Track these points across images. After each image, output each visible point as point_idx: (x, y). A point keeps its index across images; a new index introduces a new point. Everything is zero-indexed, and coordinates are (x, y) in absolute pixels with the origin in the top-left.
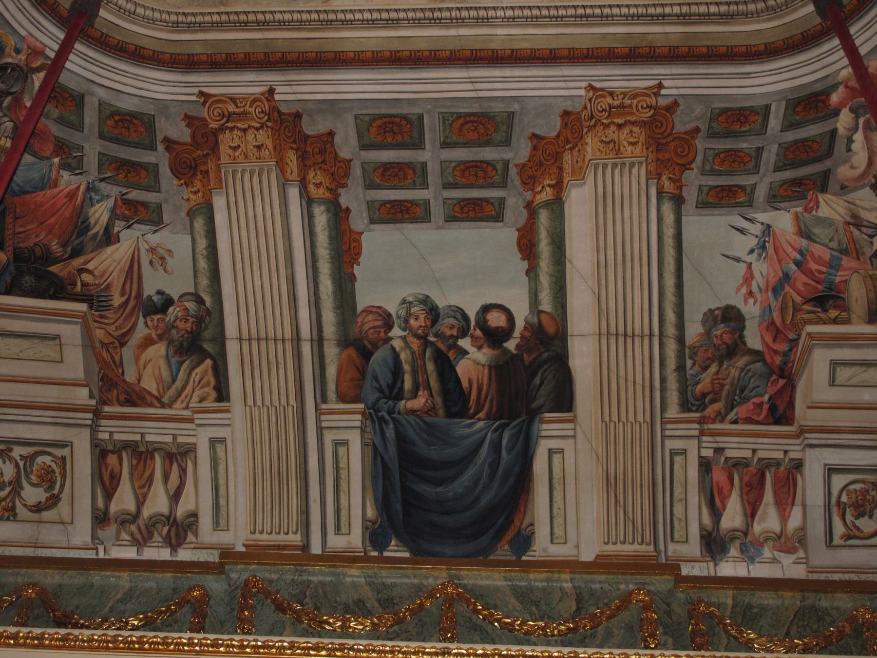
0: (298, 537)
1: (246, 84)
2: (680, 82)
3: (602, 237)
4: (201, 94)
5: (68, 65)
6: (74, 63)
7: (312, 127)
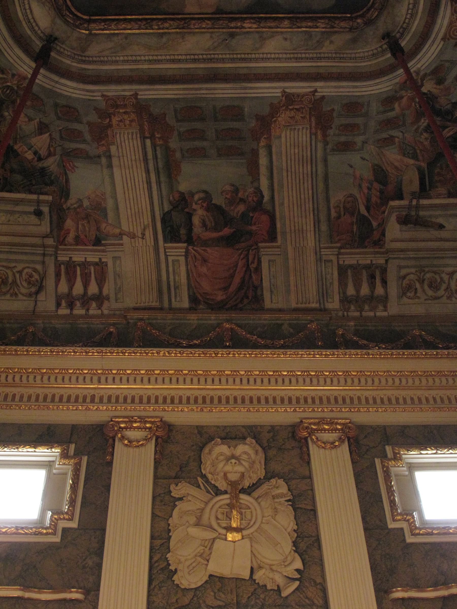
0: (158, 304)
1: (126, 90)
2: (325, 89)
3: (128, 204)
4: (103, 96)
5: (37, 81)
6: (40, 80)
7: (156, 111)
